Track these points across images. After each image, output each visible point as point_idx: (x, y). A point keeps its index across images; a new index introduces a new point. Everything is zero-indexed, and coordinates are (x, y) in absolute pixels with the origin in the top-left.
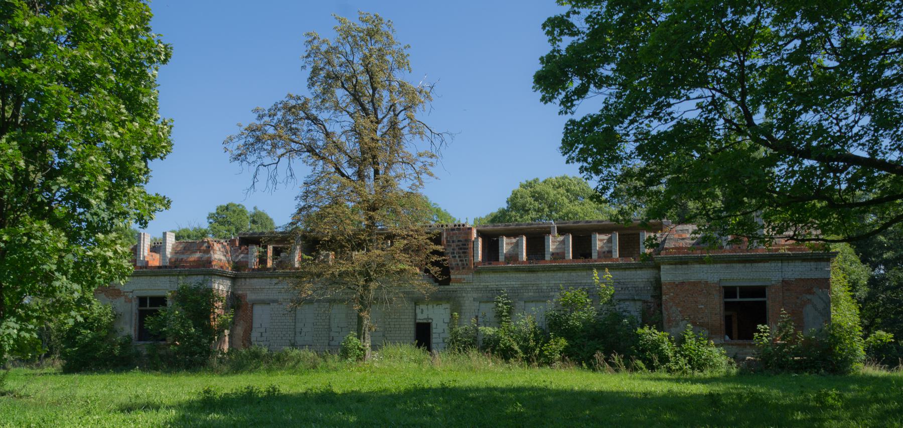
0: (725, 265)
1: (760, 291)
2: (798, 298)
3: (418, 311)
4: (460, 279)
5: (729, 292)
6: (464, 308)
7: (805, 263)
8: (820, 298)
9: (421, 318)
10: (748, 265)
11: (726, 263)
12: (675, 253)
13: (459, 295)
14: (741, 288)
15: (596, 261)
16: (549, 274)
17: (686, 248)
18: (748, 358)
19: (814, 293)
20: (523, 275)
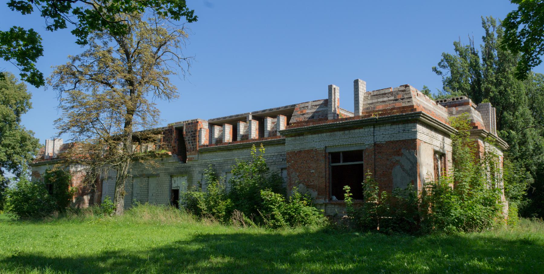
0: (329, 134)
1: (357, 155)
2: (388, 160)
3: (173, 182)
4: (192, 158)
5: (335, 156)
6: (194, 178)
7: (394, 126)
8: (407, 158)
9: (174, 186)
10: (347, 132)
11: (330, 132)
12: (295, 127)
13: (191, 169)
14: (344, 153)
15: (266, 139)
16: (240, 151)
17: (305, 122)
18: (344, 216)
19: (401, 155)
20: (224, 153)
